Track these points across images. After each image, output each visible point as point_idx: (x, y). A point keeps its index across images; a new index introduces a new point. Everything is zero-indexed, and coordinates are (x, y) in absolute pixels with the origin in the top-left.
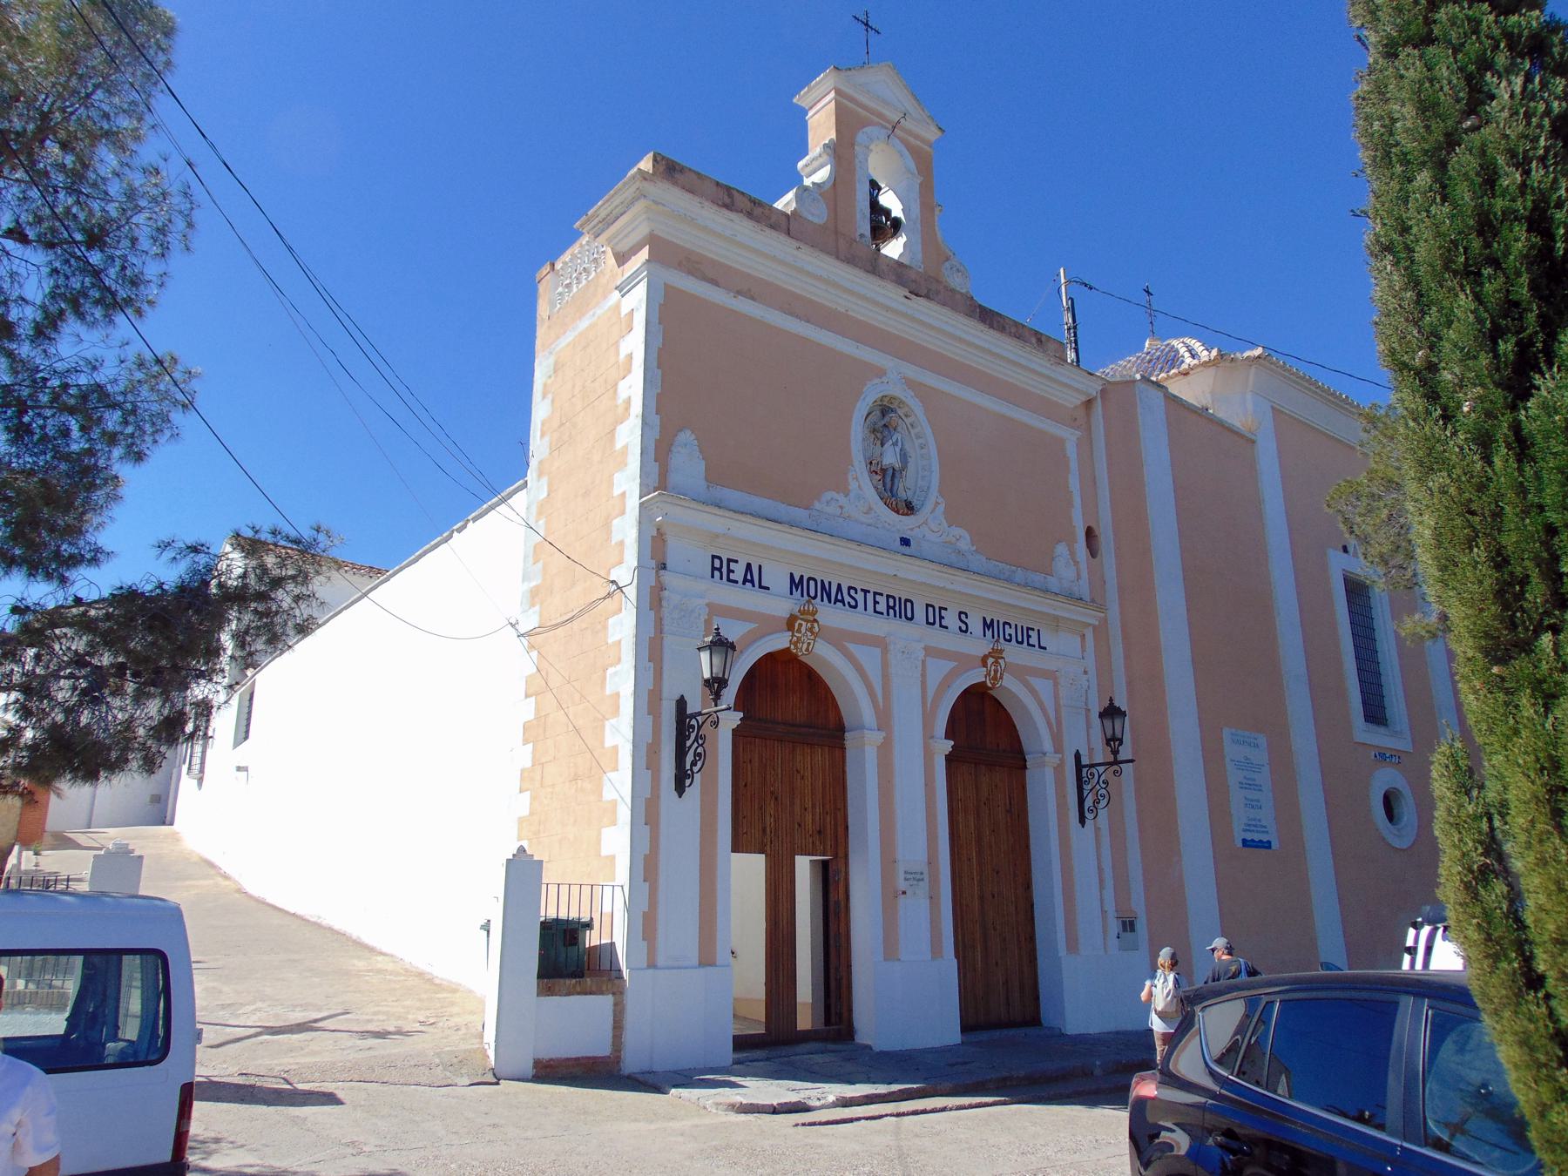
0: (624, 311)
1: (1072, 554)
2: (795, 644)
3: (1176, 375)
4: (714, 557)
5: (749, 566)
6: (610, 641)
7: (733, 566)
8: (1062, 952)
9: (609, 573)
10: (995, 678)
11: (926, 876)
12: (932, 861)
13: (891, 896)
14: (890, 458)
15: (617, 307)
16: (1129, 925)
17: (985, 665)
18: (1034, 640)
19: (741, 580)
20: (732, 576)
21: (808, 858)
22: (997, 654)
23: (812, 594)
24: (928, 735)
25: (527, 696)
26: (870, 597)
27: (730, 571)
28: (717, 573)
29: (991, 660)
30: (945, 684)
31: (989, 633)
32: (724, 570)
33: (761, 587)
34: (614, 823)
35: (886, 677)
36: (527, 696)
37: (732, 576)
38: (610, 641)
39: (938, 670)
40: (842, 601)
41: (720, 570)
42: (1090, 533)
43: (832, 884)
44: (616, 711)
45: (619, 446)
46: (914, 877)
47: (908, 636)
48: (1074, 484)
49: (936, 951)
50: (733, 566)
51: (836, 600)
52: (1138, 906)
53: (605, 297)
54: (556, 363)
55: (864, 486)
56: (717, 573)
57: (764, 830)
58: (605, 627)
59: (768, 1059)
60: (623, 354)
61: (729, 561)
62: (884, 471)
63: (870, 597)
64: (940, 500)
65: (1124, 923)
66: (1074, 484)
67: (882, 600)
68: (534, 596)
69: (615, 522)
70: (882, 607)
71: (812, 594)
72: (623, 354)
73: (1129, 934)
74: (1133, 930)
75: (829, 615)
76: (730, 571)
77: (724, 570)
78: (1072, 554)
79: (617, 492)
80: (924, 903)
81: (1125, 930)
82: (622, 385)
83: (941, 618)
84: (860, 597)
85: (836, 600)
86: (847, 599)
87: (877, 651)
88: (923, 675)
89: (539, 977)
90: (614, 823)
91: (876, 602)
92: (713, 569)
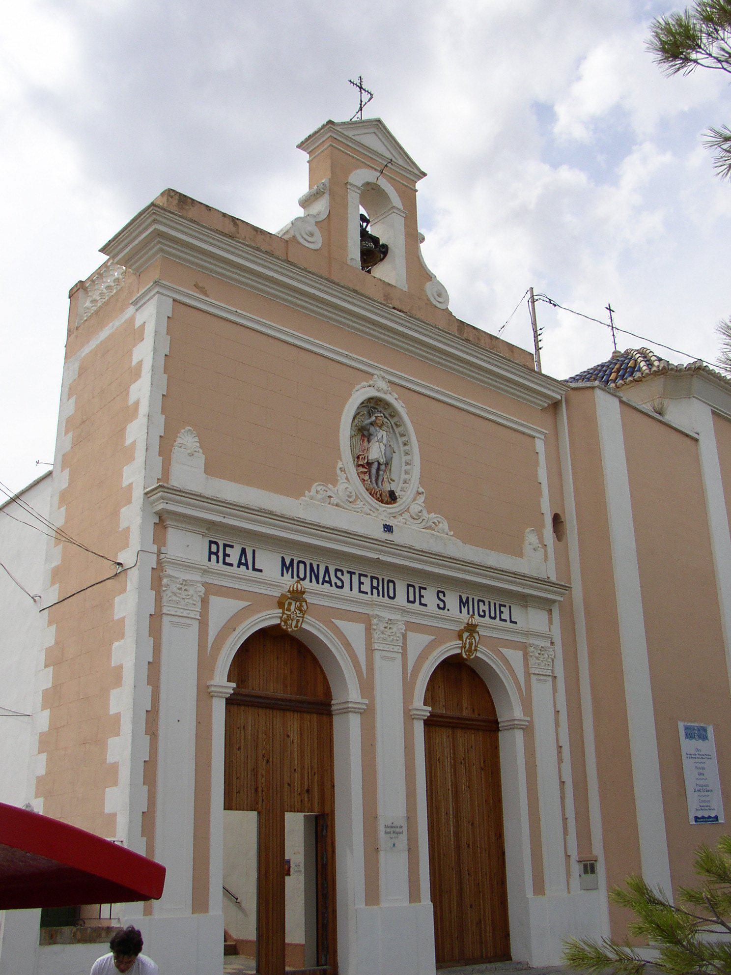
0: (138, 324)
1: (541, 539)
2: (285, 622)
3: (631, 382)
4: (211, 542)
5: (243, 551)
6: (116, 618)
7: (502, 609)
8: (530, 894)
9: (116, 557)
10: (470, 650)
11: (405, 829)
12: (411, 818)
13: (372, 851)
14: (375, 452)
15: (132, 320)
16: (589, 868)
17: (460, 637)
18: (505, 616)
19: (236, 564)
20: (228, 560)
21: (301, 815)
22: (471, 629)
23: (302, 576)
24: (205, 666)
25: (46, 666)
26: (355, 578)
27: (226, 555)
28: (214, 557)
29: (466, 635)
30: (422, 657)
31: (465, 610)
32: (221, 554)
33: (254, 569)
34: (115, 783)
35: (370, 651)
36: (46, 666)
37: (228, 560)
38: (116, 618)
39: (417, 641)
40: (330, 582)
41: (216, 554)
42: (557, 520)
43: (322, 833)
44: (118, 680)
45: (128, 442)
46: (393, 830)
47: (391, 611)
48: (542, 475)
49: (414, 896)
50: (502, 609)
51: (324, 581)
52: (598, 850)
53: (122, 310)
54: (80, 368)
55: (350, 481)
56: (214, 557)
57: (256, 790)
58: (112, 605)
59: (514, 720)
60: (135, 361)
61: (225, 546)
62: (369, 464)
63: (355, 578)
65: (585, 866)
66: (542, 475)
67: (366, 581)
68: (57, 575)
69: (123, 510)
70: (366, 587)
71: (302, 576)
72: (135, 361)
73: (589, 876)
74: (593, 871)
76: (226, 555)
77: (221, 554)
78: (541, 539)
79: (125, 484)
80: (403, 858)
81: (586, 872)
82: (134, 388)
83: (421, 596)
84: (346, 578)
85: (324, 581)
86: (334, 580)
87: (361, 627)
88: (404, 647)
89: (42, 926)
90: (115, 783)
91: (361, 583)
92: (211, 553)
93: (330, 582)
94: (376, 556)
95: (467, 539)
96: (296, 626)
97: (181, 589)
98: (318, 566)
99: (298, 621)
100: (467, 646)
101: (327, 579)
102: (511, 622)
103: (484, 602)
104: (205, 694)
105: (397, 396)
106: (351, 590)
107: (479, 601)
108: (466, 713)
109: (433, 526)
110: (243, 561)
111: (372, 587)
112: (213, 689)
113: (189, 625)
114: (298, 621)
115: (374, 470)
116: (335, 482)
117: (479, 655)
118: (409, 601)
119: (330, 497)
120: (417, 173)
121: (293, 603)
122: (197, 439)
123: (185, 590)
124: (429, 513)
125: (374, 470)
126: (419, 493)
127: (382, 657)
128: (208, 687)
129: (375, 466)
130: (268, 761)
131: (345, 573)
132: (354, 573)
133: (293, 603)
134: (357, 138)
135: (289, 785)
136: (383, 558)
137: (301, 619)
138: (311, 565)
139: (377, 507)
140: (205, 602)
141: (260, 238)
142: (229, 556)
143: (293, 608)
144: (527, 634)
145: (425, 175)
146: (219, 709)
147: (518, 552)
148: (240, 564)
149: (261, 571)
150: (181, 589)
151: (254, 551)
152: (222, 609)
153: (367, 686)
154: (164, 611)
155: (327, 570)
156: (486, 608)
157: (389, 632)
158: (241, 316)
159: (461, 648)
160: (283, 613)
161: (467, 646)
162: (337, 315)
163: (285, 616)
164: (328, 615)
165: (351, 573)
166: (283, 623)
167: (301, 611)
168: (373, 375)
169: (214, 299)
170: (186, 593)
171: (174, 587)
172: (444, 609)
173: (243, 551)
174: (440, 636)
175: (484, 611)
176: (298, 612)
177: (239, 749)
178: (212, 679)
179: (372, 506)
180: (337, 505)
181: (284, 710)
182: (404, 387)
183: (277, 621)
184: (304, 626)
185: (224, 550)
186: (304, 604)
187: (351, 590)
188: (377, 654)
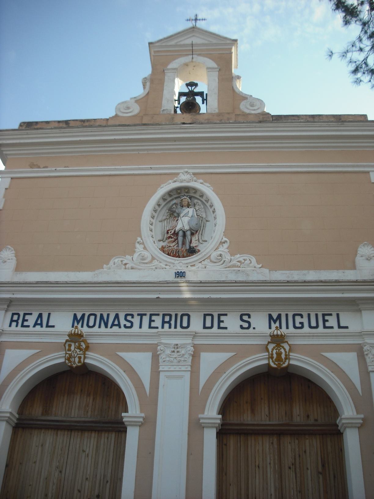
5: (40, 316)
19: (160, 325)
20: (327, 324)
26: (146, 320)
27: (24, 320)
29: (271, 347)
32: (20, 321)
40: (119, 325)
50: (27, 317)
51: (113, 325)
62: (176, 234)
63: (146, 320)
64: (225, 239)
70: (158, 321)
75: (96, 334)
77: (20, 321)
84: (136, 320)
85: (113, 325)
86: (123, 322)
92: (12, 321)
93: (119, 325)
94: (155, 296)
95: (273, 268)
96: (80, 362)
97: (174, 352)
98: (108, 315)
99: (80, 358)
100: (275, 356)
101: (39, 322)
102: (340, 327)
103: (302, 316)
104: (196, 426)
105: (201, 181)
106: (140, 327)
107: (294, 316)
108: (297, 419)
109: (239, 264)
110: (39, 322)
111: (164, 322)
112: (201, 421)
113: (181, 377)
114: (80, 358)
115: (180, 239)
116: (132, 252)
117: (292, 362)
118: (205, 327)
119: (126, 264)
120: (228, 42)
121: (73, 345)
122: (14, 252)
123: (178, 352)
124: (232, 254)
125: (180, 239)
126: (222, 243)
127: (167, 377)
128: (199, 419)
129: (181, 233)
130: (61, 472)
131: (136, 316)
132: (145, 315)
133: (73, 345)
134: (182, 43)
135: (79, 491)
136: (161, 296)
137: (82, 356)
138: (102, 315)
139: (173, 261)
140: (195, 356)
141: (320, 118)
142: (223, 321)
143: (73, 348)
144: (361, 334)
145: (236, 41)
146: (210, 439)
147: (354, 267)
148: (36, 324)
149: (347, 327)
150: (174, 352)
151: (49, 314)
152: (210, 362)
153: (150, 402)
154: (160, 369)
155: (117, 316)
156: (305, 321)
157: (176, 355)
158: (21, 172)
159: (269, 358)
160: (66, 353)
161: (275, 356)
162: (350, 142)
163: (67, 355)
164: (112, 351)
165: (141, 315)
166: (67, 361)
167: (81, 350)
168: (178, 174)
169: (101, 166)
170: (178, 354)
171: (168, 352)
172: (248, 328)
173: (40, 316)
174: (241, 351)
175: (302, 323)
176: (78, 351)
177: (35, 462)
178: (203, 413)
179: (197, 260)
180: (132, 269)
181: (98, 431)
182: (212, 173)
183: (62, 360)
184: (87, 361)
185: (219, 318)
186: (82, 344)
187: (140, 327)
188: (162, 375)
